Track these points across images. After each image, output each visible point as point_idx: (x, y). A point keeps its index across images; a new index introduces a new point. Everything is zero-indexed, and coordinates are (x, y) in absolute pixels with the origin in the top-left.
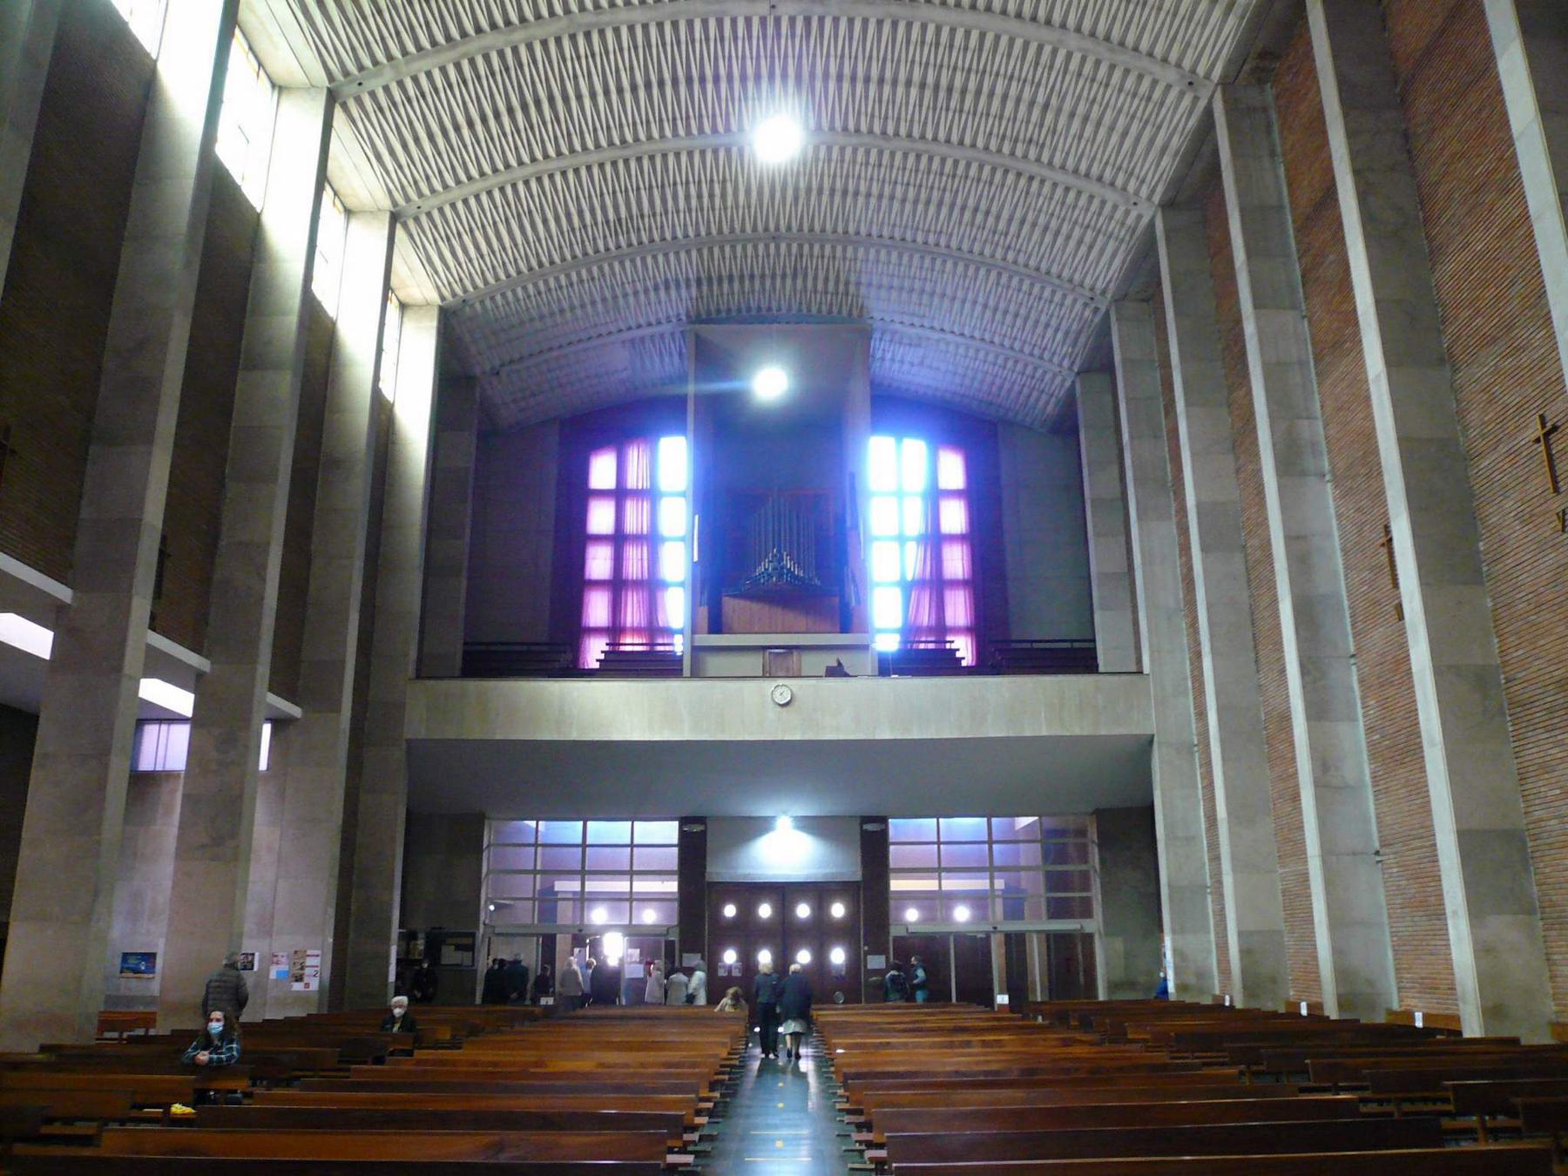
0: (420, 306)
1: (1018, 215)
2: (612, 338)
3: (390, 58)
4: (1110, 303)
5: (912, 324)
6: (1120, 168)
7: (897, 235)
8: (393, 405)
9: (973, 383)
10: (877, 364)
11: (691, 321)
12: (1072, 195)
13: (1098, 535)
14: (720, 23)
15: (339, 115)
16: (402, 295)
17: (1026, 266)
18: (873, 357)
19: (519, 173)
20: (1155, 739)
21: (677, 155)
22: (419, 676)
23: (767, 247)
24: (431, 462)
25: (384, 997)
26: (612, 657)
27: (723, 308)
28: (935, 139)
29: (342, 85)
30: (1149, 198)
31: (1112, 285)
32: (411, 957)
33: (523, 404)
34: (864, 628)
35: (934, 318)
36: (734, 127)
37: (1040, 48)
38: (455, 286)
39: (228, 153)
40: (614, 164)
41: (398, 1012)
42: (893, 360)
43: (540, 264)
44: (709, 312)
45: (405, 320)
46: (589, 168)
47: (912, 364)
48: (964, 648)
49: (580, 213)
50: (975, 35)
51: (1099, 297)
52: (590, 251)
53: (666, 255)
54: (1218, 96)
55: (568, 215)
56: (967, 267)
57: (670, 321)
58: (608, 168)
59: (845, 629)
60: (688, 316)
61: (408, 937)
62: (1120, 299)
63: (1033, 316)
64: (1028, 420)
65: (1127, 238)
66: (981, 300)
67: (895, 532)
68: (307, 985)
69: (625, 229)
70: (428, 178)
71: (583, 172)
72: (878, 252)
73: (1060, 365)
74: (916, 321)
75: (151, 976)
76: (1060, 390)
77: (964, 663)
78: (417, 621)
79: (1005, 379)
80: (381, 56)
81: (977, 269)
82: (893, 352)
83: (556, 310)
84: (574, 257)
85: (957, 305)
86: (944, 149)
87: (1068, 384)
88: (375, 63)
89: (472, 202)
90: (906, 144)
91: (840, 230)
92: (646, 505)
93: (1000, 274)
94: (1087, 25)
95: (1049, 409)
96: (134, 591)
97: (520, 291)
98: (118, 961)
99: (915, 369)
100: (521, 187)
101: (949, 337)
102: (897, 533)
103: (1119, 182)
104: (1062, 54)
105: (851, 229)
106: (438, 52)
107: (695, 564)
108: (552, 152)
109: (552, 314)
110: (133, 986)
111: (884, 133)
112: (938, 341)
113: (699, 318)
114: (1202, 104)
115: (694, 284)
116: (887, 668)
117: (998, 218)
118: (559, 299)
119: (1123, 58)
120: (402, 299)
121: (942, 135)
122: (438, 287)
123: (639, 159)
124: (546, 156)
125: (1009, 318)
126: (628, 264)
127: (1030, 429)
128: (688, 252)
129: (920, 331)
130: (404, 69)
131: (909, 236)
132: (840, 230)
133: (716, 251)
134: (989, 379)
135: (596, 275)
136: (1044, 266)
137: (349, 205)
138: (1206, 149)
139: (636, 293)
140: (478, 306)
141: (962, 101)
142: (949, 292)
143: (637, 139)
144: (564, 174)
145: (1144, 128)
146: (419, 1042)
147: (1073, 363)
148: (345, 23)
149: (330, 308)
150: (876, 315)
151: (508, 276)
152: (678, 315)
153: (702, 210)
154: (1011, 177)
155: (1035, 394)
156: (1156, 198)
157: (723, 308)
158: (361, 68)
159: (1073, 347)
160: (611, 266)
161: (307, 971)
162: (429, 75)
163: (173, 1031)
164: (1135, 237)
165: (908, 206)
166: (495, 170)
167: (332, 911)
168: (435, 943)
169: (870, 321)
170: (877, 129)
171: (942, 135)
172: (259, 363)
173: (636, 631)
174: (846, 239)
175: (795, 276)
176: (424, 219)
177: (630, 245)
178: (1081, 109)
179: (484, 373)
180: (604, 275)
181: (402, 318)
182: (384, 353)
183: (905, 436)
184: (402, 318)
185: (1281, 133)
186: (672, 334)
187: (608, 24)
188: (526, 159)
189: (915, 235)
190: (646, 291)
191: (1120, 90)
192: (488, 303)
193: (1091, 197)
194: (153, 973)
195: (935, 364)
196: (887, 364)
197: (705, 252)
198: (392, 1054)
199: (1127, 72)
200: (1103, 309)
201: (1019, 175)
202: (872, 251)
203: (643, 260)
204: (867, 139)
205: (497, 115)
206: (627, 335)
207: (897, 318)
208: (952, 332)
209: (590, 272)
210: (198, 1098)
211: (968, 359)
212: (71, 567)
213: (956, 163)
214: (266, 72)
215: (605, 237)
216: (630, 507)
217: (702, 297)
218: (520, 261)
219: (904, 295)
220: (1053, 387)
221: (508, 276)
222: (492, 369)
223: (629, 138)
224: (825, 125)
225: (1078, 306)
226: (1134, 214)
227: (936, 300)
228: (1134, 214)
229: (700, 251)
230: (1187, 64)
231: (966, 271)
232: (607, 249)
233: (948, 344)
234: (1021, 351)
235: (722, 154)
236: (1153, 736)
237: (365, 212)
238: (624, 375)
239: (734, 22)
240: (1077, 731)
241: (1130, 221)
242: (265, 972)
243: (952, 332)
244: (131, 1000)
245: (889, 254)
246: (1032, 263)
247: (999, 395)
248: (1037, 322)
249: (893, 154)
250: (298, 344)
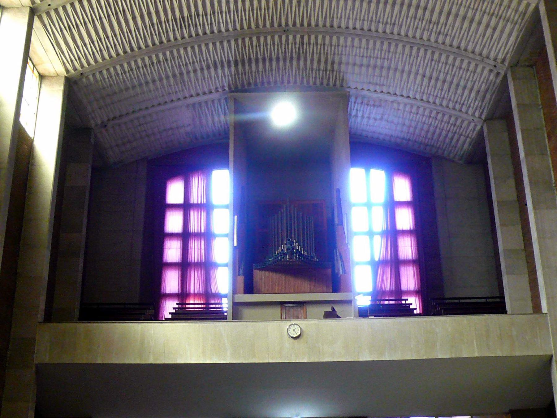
0: (53, 77)
1: (446, 9)
2: (180, 103)
4: (507, 68)
5: (375, 91)
8: (33, 141)
11: (231, 91)
13: (502, 225)
17: (451, 45)
18: (350, 115)
20: (554, 358)
26: (181, 311)
31: (509, 55)
34: (349, 289)
42: (363, 117)
43: (132, 49)
45: (43, 85)
47: (376, 120)
48: (414, 302)
51: (500, 64)
53: (214, 44)
55: (149, 14)
57: (218, 91)
59: (336, 290)
62: (514, 66)
64: (452, 155)
65: (520, 20)
66: (421, 71)
67: (367, 229)
69: (187, 24)
72: (353, 40)
73: (473, 115)
74: (378, 88)
76: (473, 134)
77: (415, 312)
79: (437, 127)
81: (419, 49)
82: (363, 111)
83: (143, 82)
85: (405, 75)
87: (478, 128)
91: (328, 24)
92: (203, 214)
93: (433, 52)
95: (466, 147)
101: (400, 99)
102: (367, 230)
105: (335, 24)
107: (235, 248)
109: (140, 85)
116: (363, 313)
120: (40, 72)
125: (439, 84)
126: (189, 50)
127: (453, 161)
129: (380, 95)
132: (328, 24)
133: (247, 40)
136: (463, 45)
139: (195, 71)
140: (91, 77)
149: (30, 132)
150: (352, 85)
151: (111, 57)
155: (456, 136)
160: (178, 51)
164: (524, 21)
169: (348, 90)
173: (196, 295)
175: (299, 59)
176: (53, 14)
179: (96, 125)
180: (174, 58)
181: (41, 84)
183: (374, 167)
184: (41, 84)
186: (219, 100)
190: (202, 69)
192: (98, 76)
195: (391, 119)
196: (359, 119)
200: (503, 73)
202: (349, 40)
203: (200, 47)
207: (365, 87)
208: (402, 96)
211: (412, 115)
215: (174, 30)
216: (193, 215)
219: (370, 70)
221: (111, 57)
222: (102, 123)
225: (486, 72)
229: (236, 41)
232: (176, 39)
233: (399, 104)
236: (552, 356)
238: (188, 129)
240: (499, 354)
241: (522, 8)
243: (402, 96)
245: (360, 40)
246: (455, 43)
247: (432, 139)
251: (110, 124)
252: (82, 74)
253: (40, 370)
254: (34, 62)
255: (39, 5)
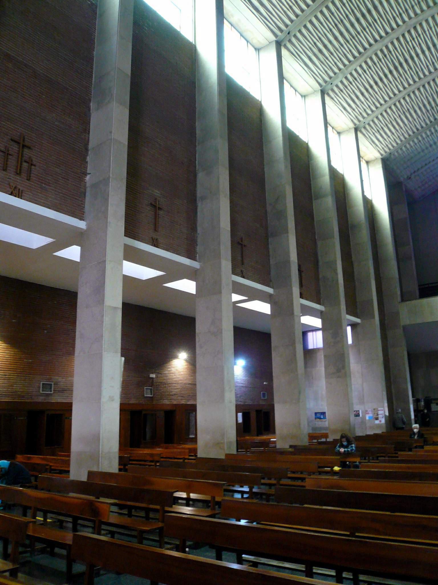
0: (374, 160)
3: (340, 69)
8: (261, 102)
16: (367, 158)
19: (400, 96)
22: (403, 300)
24: (391, 219)
25: (411, 425)
32: (419, 409)
33: (423, 188)
38: (385, 149)
39: (291, 125)
41: (415, 430)
43: (418, 130)
45: (369, 167)
49: (429, 103)
55: (424, 106)
61: (417, 401)
68: (380, 421)
70: (365, 110)
71: (427, 86)
75: (325, 420)
78: (398, 280)
80: (336, 70)
84: (431, 122)
88: (335, 74)
89: (384, 114)
96: (292, 285)
97: (411, 143)
98: (314, 415)
100: (402, 101)
108: (411, 82)
109: (427, 148)
110: (319, 423)
118: (428, 141)
122: (379, 151)
124: (409, 85)
130: (346, 71)
137: (339, 131)
140: (396, 154)
146: (426, 442)
148: (320, 63)
151: (405, 138)
158: (330, 78)
161: (380, 416)
162: (356, 70)
163: (334, 439)
166: (390, 98)
167: (385, 393)
168: (428, 403)
172: (319, 197)
176: (367, 126)
181: (368, 166)
182: (363, 182)
184: (368, 166)
187: (422, 20)
192: (400, 151)
194: (326, 419)
198: (416, 447)
205: (386, 76)
210: (343, 465)
212: (271, 281)
214: (251, 44)
221: (405, 138)
222: (408, 177)
237: (262, 48)
242: (364, 417)
244: (321, 428)
251: (413, 176)
252: (390, 153)
253: (405, 328)
254: (332, 125)
255: (359, 125)
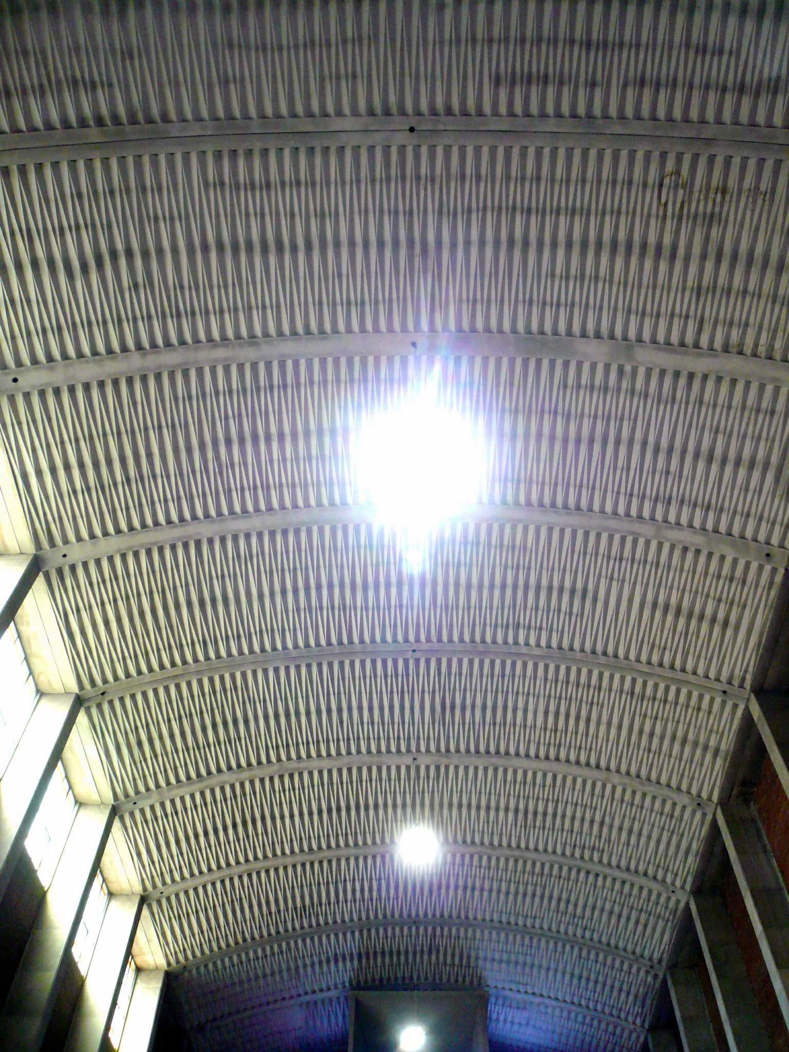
0: (151, 971)
2: (292, 1002)
3: (158, 786)
6: (658, 866)
7: (504, 920)
9: (568, 1040)
10: (493, 1025)
12: (627, 887)
14: (379, 769)
15: (117, 825)
16: (139, 961)
18: (491, 1019)
21: (348, 860)
23: (410, 929)
27: (377, 977)
28: (527, 848)
29: (123, 803)
30: (683, 888)
31: (665, 955)
35: (534, 985)
36: (387, 840)
37: (594, 785)
40: (303, 865)
43: (245, 940)
44: (366, 981)
45: (138, 981)
46: (285, 868)
50: (549, 776)
52: (281, 930)
53: (336, 935)
54: (719, 812)
55: (268, 902)
56: (556, 943)
58: (299, 868)
60: (350, 982)
62: (672, 967)
63: (609, 982)
65: (671, 918)
70: (171, 871)
71: (281, 871)
73: (634, 1023)
80: (152, 785)
84: (269, 934)
86: (534, 855)
87: (642, 1039)
88: (148, 789)
90: (508, 852)
91: (463, 916)
94: (623, 768)
97: (227, 960)
99: (522, 1030)
100: (236, 881)
101: (547, 1001)
103: (660, 876)
104: (609, 788)
106: (191, 784)
111: (491, 844)
112: (539, 1005)
113: (357, 986)
114: (709, 818)
115: (356, 958)
117: (576, 906)
119: (650, 789)
121: (531, 846)
123: (321, 862)
124: (256, 858)
126: (308, 941)
128: (353, 933)
131: (512, 921)
132: (463, 916)
134: (580, 1036)
135: (284, 949)
137: (80, 799)
138: (717, 849)
140: (194, 971)
141: (544, 821)
142: (544, 964)
143: (320, 848)
144: (267, 871)
145: (595, 423)
147: (644, 1021)
149: (82, 968)
150: (489, 982)
151: (220, 948)
152: (344, 983)
153: (364, 901)
154: (582, 875)
156: (688, 887)
157: (377, 977)
158: (137, 792)
159: (643, 1007)
162: (182, 799)
165: (511, 897)
169: (487, 989)
170: (486, 841)
171: (531, 846)
174: (467, 923)
175: (430, 953)
177: (311, 926)
178: (626, 825)
185: (768, 835)
186: (338, 998)
187: (305, 769)
188: (242, 860)
189: (517, 919)
190: (320, 963)
191: (652, 811)
192: (202, 969)
193: (641, 888)
196: (501, 1023)
197: (365, 932)
199: (654, 798)
200: (661, 975)
201: (588, 872)
204: (479, 849)
206: (305, 998)
208: (549, 997)
209: (280, 946)
213: (543, 865)
217: (361, 969)
218: (229, 937)
220: (631, 1042)
221: (220, 948)
223: (315, 847)
224: (450, 839)
225: (642, 974)
226: (673, 899)
227: (535, 970)
228: (673, 899)
229: (361, 932)
230: (694, 791)
231: (556, 947)
233: (547, 1007)
234: (603, 1012)
235: (378, 860)
238: (299, 1033)
239: (389, 768)
241: (671, 905)
243: (549, 997)
248: (612, 987)
249: (498, 859)
250: (52, 995)
